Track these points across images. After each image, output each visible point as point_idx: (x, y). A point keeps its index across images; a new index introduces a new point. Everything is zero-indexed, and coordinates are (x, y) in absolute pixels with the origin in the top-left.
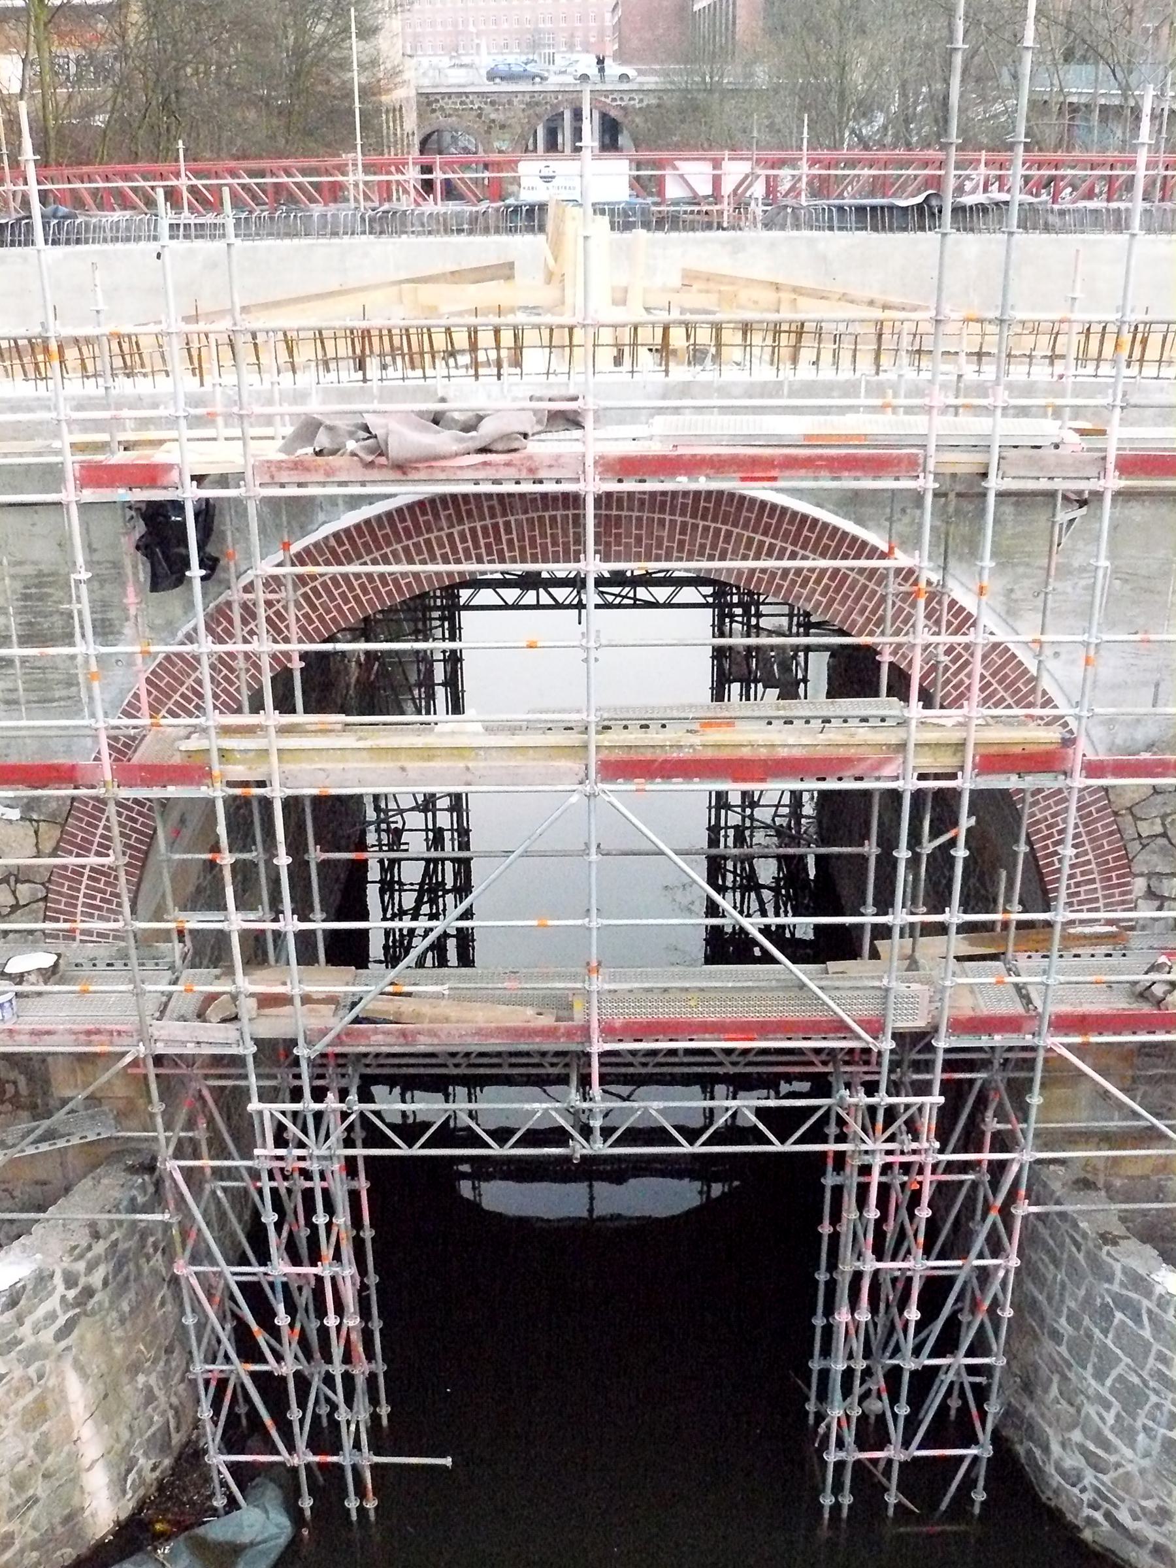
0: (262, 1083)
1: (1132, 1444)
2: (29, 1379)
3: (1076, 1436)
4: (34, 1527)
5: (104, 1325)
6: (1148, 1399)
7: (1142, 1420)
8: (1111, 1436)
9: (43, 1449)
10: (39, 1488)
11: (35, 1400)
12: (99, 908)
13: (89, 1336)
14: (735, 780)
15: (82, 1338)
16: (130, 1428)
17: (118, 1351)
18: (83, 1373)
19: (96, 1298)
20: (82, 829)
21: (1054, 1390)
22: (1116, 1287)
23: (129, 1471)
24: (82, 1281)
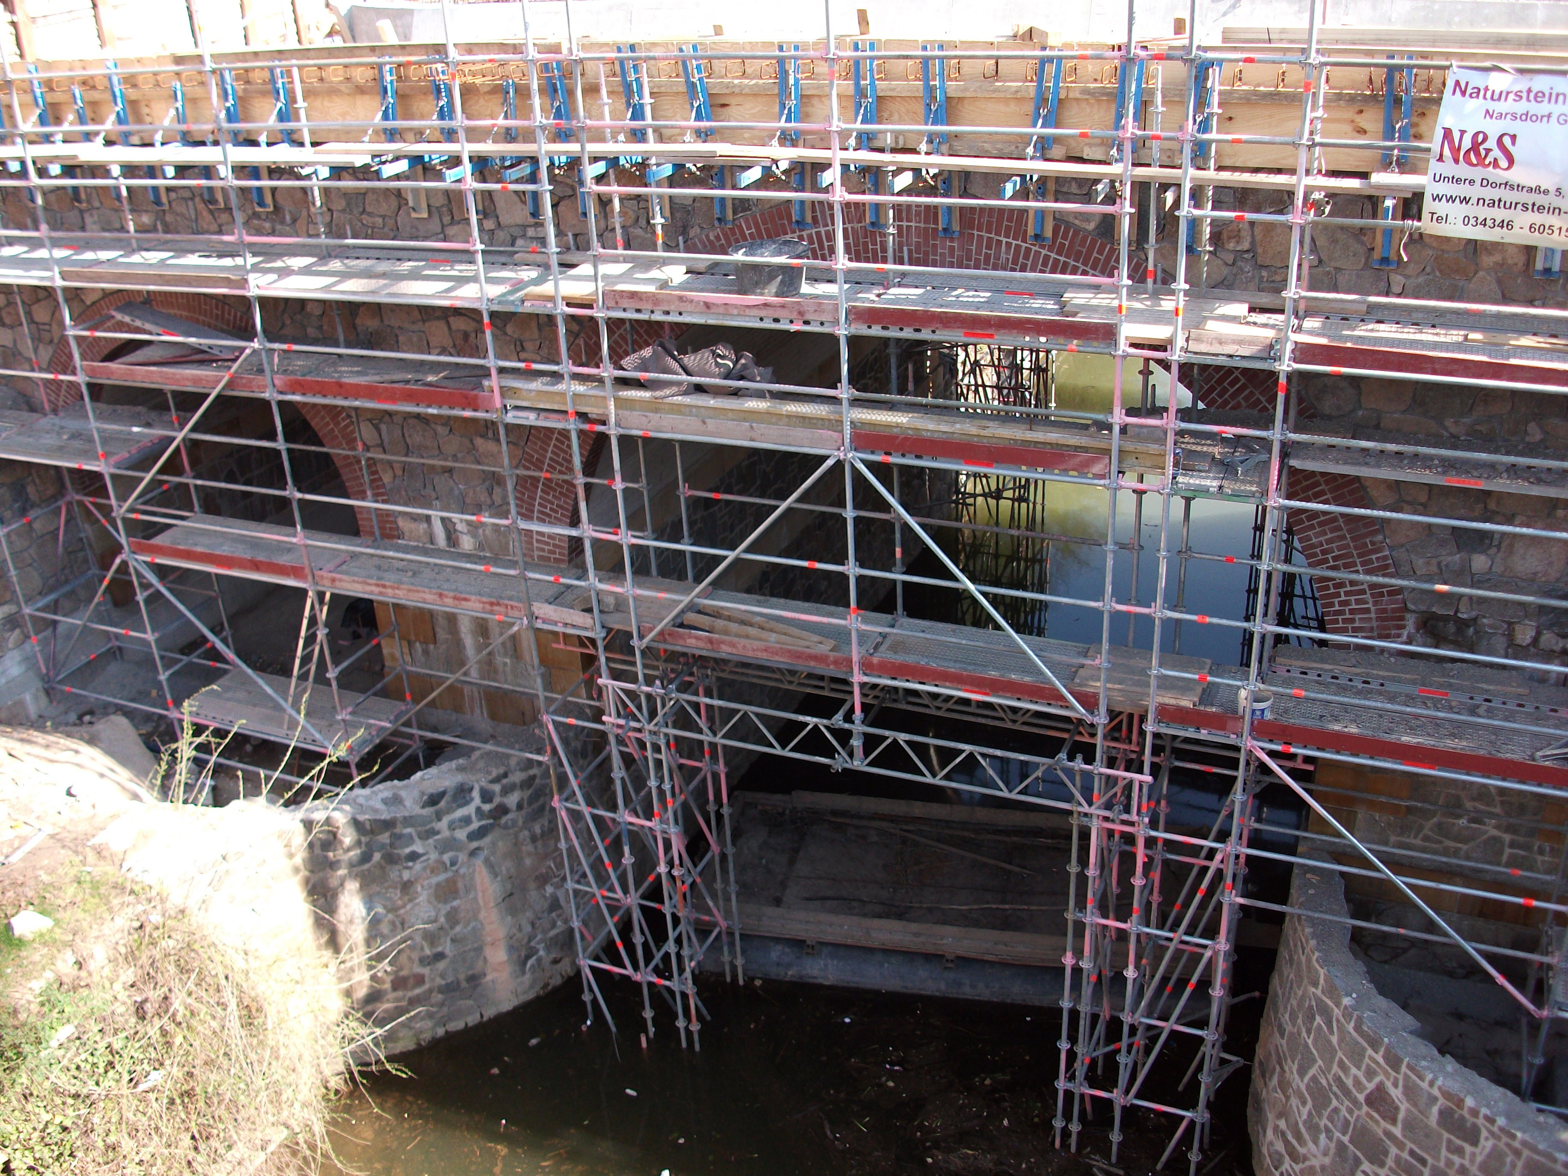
0: (647, 671)
1: (1316, 1142)
2: (444, 863)
3: (1282, 1124)
4: (442, 976)
5: (516, 837)
6: (1330, 1102)
7: (1324, 1122)
8: (1303, 1130)
9: (453, 918)
10: (447, 947)
11: (447, 880)
12: (549, 516)
13: (500, 844)
14: (967, 462)
15: (494, 844)
16: (533, 924)
17: (528, 862)
18: (494, 872)
19: (510, 816)
20: (536, 452)
21: (1275, 1081)
22: (1319, 992)
23: (528, 957)
24: (497, 800)
